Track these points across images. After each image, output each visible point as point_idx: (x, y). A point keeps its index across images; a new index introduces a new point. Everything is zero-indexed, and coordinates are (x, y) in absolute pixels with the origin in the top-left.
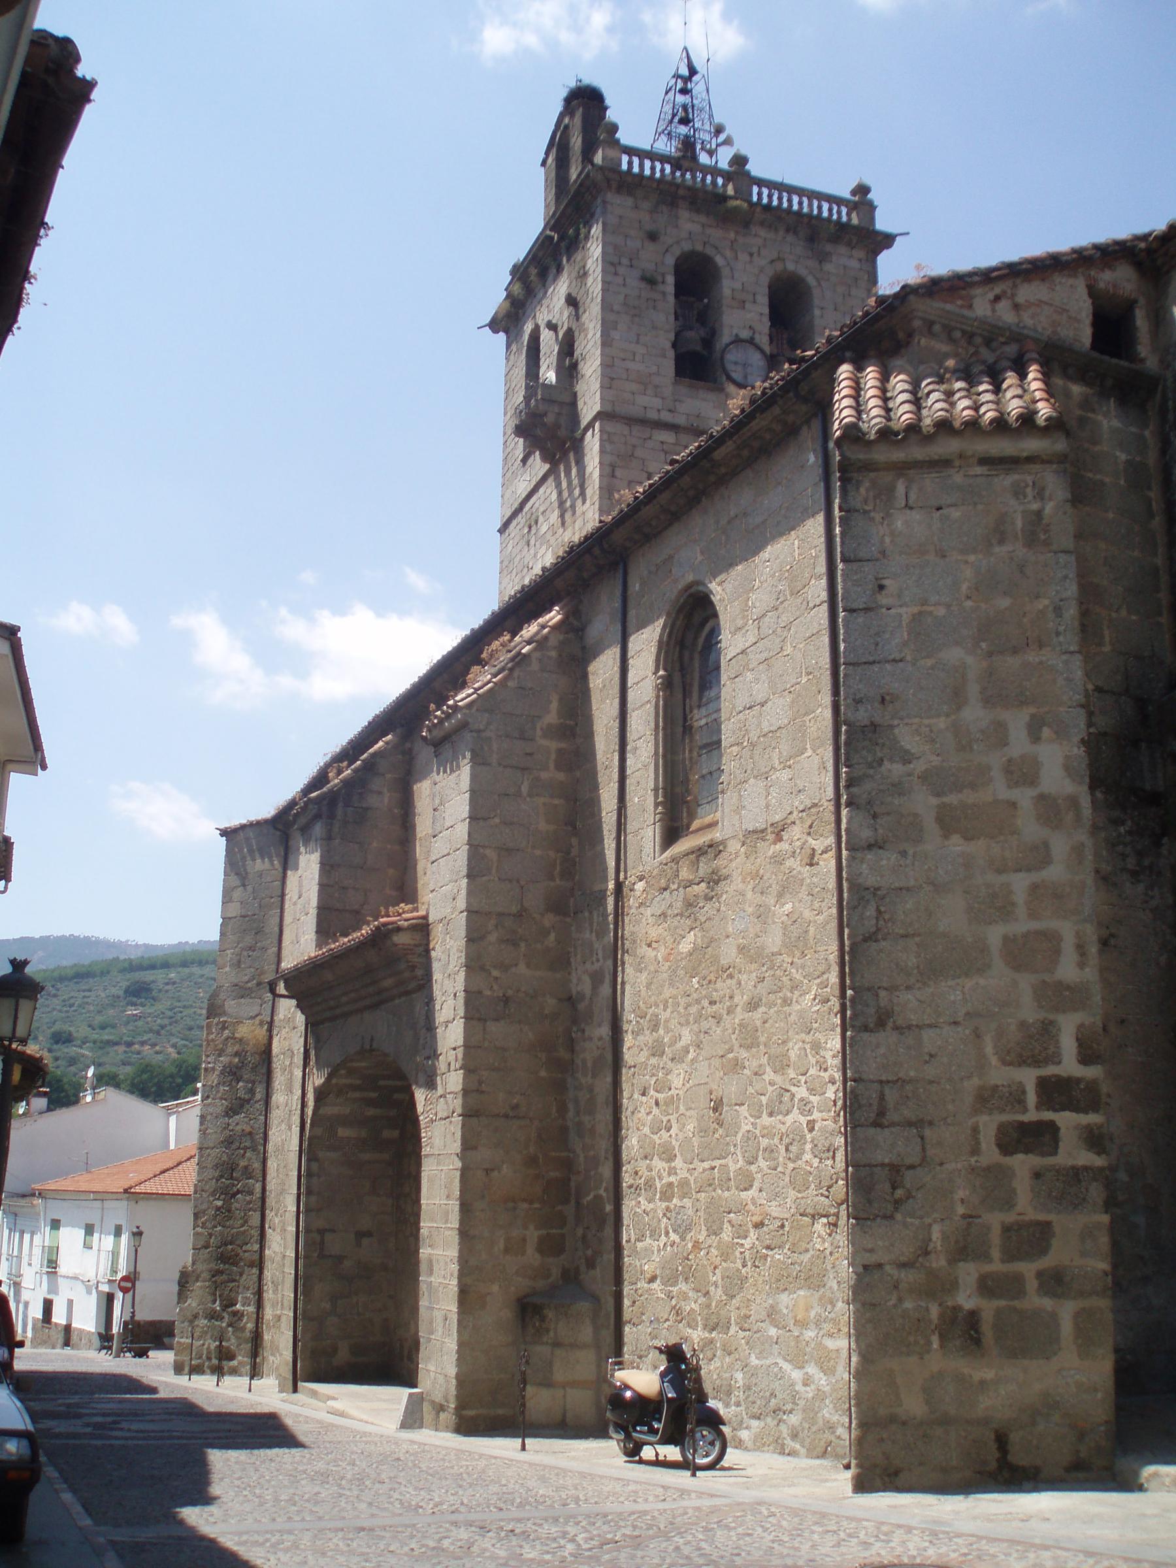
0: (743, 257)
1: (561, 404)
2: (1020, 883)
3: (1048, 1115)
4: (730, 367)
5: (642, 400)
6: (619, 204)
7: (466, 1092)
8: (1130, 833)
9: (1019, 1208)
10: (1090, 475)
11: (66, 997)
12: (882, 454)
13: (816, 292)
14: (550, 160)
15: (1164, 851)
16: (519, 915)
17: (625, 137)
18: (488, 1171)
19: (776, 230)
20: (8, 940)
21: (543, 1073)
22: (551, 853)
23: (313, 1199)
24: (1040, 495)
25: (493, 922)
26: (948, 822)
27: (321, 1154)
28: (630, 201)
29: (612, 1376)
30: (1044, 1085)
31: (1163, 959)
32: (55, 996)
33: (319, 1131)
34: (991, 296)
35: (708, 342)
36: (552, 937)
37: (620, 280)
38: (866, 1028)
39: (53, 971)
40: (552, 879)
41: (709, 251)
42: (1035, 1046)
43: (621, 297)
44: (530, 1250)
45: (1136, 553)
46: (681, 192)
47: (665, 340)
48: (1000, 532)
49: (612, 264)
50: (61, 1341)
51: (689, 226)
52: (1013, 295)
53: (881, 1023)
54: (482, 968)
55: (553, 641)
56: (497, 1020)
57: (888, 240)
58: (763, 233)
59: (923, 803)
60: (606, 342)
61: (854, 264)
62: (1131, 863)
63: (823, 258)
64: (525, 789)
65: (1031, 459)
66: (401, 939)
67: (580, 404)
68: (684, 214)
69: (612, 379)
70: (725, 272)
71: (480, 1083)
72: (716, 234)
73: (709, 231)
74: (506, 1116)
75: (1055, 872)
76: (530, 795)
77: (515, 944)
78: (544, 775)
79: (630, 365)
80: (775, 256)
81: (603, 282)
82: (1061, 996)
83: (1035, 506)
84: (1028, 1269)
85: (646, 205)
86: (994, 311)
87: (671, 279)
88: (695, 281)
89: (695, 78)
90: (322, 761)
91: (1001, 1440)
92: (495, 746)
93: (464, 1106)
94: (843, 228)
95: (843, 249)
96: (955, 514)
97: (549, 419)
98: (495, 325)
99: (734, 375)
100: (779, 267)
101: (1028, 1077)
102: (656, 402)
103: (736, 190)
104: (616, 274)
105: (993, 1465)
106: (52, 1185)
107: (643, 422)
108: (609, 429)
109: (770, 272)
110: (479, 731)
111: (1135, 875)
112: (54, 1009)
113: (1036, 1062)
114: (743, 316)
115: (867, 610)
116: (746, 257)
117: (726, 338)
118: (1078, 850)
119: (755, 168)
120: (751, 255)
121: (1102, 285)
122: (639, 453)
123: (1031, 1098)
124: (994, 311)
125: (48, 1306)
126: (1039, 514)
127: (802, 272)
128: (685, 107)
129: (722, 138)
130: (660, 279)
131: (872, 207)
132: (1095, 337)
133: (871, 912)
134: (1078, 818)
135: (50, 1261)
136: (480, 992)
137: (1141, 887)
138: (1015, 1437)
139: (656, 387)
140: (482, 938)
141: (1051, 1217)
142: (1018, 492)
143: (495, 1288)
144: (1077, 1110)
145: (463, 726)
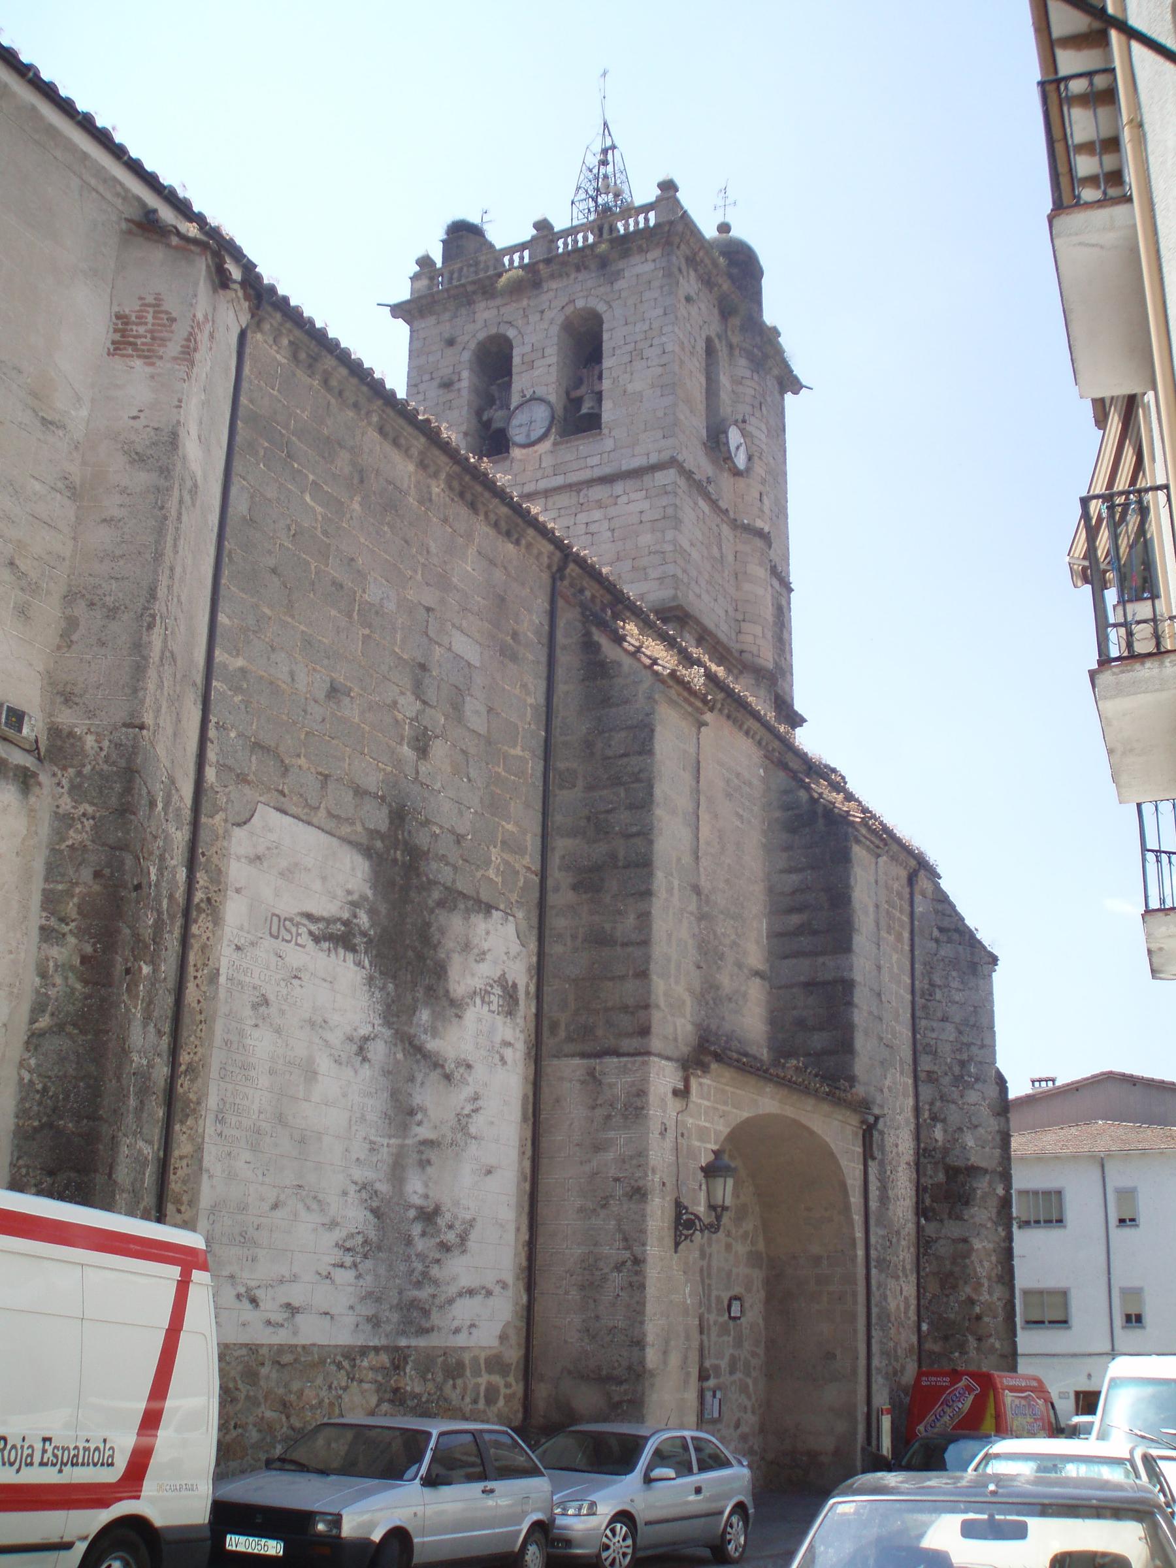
29: (115, 1559)
46: (470, 288)
51: (487, 315)
58: (554, 285)
90: (251, 252)
100: (569, 310)
109: (560, 319)
116: (537, 317)
130: (456, 378)
134: (389, 505)
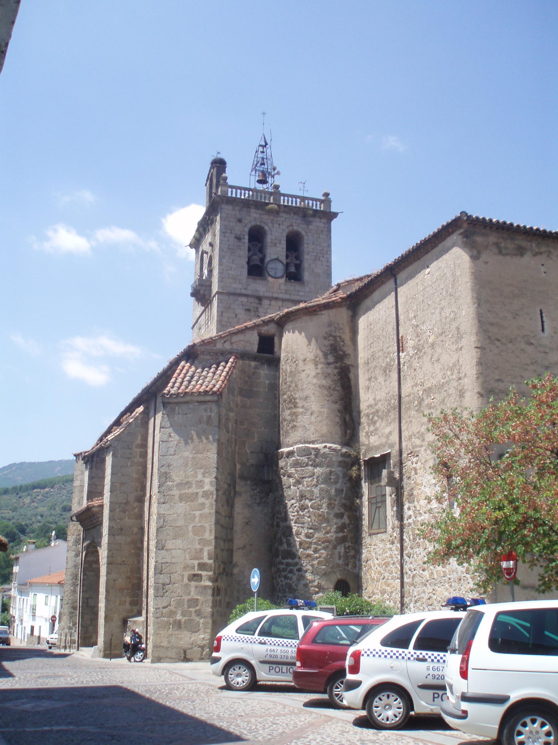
0: (276, 226)
1: (206, 286)
2: (197, 513)
3: (200, 572)
4: (269, 270)
5: (234, 286)
6: (227, 209)
7: (108, 557)
8: (258, 492)
9: (192, 595)
10: (255, 389)
11: (69, 489)
12: (171, 400)
13: (305, 237)
14: (208, 184)
15: (270, 497)
16: (126, 504)
17: (230, 182)
18: (114, 581)
19: (290, 214)
20: (43, 462)
21: (133, 551)
22: (137, 484)
23: (85, 588)
24: (211, 411)
25: (118, 505)
26: (181, 498)
27: (87, 573)
28: (231, 207)
30: (199, 564)
31: (267, 527)
32: (64, 489)
33: (87, 566)
34: (223, 341)
35: (262, 260)
36: (137, 509)
37: (226, 239)
38: (159, 550)
39: (63, 477)
40: (137, 491)
41: (263, 225)
42: (197, 555)
43: (227, 245)
44: (127, 604)
45: (269, 411)
46: (251, 202)
47: (244, 262)
48: (200, 421)
49: (224, 233)
50: (37, 642)
51: (255, 215)
52: (231, 340)
53: (163, 549)
54: (114, 519)
55: (140, 418)
56: (118, 535)
57: (335, 215)
58: (284, 215)
59: (176, 492)
60: (220, 264)
61: (322, 225)
62: (258, 501)
63: (309, 223)
64: (129, 464)
65: (209, 401)
66: (94, 509)
67: (212, 287)
68: (253, 210)
69: (222, 278)
70: (269, 232)
71: (112, 554)
72: (265, 217)
73: (262, 216)
74: (121, 564)
75: (206, 510)
76: (131, 466)
77: (125, 512)
78: (135, 460)
79: (230, 272)
80: (289, 224)
81: (220, 240)
82: (203, 542)
83: (209, 414)
84: (193, 610)
85: (238, 208)
86: (223, 346)
87: (247, 237)
88: (257, 237)
89: (267, 146)
91: (185, 652)
92: (120, 452)
93: (107, 561)
94: (316, 213)
95: (317, 219)
96: (190, 416)
97: (202, 292)
98: (191, 246)
99: (271, 273)
100: (291, 228)
101: (196, 562)
102: (240, 286)
103: (274, 199)
104: (225, 236)
105: (182, 658)
106: (34, 580)
107: (234, 294)
108: (220, 297)
109: (287, 231)
110: (115, 447)
111: (259, 504)
112: (63, 495)
113: (198, 559)
114: (276, 250)
115: (166, 442)
117: (267, 259)
118: (211, 505)
119: (282, 190)
120: (279, 225)
121: (263, 331)
122: (232, 306)
123: (196, 568)
124: (223, 346)
125: (32, 628)
126: (210, 416)
127: (300, 230)
128: (263, 159)
129: (276, 172)
131: (330, 201)
132: (259, 348)
133: (162, 520)
135: (33, 609)
136: (113, 527)
137: (261, 507)
138: (188, 651)
139: (240, 280)
140: (114, 510)
141: (199, 597)
142: (205, 410)
143: (116, 615)
144: (207, 571)
145: (110, 446)
